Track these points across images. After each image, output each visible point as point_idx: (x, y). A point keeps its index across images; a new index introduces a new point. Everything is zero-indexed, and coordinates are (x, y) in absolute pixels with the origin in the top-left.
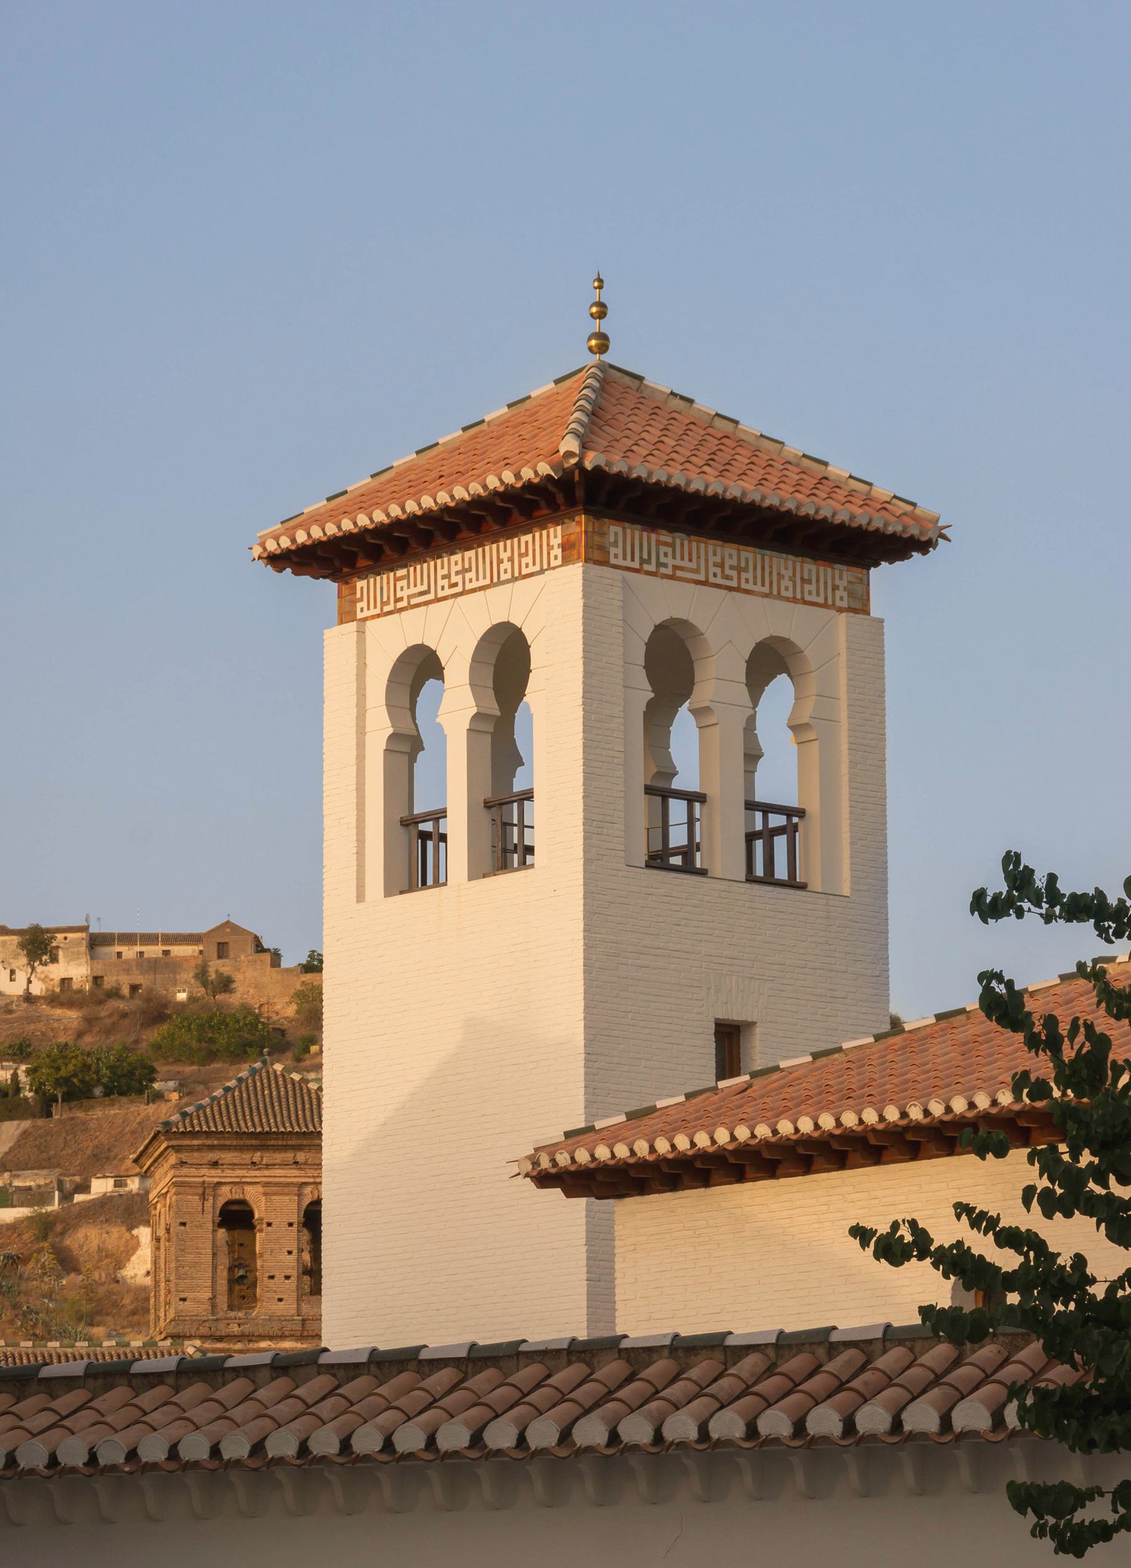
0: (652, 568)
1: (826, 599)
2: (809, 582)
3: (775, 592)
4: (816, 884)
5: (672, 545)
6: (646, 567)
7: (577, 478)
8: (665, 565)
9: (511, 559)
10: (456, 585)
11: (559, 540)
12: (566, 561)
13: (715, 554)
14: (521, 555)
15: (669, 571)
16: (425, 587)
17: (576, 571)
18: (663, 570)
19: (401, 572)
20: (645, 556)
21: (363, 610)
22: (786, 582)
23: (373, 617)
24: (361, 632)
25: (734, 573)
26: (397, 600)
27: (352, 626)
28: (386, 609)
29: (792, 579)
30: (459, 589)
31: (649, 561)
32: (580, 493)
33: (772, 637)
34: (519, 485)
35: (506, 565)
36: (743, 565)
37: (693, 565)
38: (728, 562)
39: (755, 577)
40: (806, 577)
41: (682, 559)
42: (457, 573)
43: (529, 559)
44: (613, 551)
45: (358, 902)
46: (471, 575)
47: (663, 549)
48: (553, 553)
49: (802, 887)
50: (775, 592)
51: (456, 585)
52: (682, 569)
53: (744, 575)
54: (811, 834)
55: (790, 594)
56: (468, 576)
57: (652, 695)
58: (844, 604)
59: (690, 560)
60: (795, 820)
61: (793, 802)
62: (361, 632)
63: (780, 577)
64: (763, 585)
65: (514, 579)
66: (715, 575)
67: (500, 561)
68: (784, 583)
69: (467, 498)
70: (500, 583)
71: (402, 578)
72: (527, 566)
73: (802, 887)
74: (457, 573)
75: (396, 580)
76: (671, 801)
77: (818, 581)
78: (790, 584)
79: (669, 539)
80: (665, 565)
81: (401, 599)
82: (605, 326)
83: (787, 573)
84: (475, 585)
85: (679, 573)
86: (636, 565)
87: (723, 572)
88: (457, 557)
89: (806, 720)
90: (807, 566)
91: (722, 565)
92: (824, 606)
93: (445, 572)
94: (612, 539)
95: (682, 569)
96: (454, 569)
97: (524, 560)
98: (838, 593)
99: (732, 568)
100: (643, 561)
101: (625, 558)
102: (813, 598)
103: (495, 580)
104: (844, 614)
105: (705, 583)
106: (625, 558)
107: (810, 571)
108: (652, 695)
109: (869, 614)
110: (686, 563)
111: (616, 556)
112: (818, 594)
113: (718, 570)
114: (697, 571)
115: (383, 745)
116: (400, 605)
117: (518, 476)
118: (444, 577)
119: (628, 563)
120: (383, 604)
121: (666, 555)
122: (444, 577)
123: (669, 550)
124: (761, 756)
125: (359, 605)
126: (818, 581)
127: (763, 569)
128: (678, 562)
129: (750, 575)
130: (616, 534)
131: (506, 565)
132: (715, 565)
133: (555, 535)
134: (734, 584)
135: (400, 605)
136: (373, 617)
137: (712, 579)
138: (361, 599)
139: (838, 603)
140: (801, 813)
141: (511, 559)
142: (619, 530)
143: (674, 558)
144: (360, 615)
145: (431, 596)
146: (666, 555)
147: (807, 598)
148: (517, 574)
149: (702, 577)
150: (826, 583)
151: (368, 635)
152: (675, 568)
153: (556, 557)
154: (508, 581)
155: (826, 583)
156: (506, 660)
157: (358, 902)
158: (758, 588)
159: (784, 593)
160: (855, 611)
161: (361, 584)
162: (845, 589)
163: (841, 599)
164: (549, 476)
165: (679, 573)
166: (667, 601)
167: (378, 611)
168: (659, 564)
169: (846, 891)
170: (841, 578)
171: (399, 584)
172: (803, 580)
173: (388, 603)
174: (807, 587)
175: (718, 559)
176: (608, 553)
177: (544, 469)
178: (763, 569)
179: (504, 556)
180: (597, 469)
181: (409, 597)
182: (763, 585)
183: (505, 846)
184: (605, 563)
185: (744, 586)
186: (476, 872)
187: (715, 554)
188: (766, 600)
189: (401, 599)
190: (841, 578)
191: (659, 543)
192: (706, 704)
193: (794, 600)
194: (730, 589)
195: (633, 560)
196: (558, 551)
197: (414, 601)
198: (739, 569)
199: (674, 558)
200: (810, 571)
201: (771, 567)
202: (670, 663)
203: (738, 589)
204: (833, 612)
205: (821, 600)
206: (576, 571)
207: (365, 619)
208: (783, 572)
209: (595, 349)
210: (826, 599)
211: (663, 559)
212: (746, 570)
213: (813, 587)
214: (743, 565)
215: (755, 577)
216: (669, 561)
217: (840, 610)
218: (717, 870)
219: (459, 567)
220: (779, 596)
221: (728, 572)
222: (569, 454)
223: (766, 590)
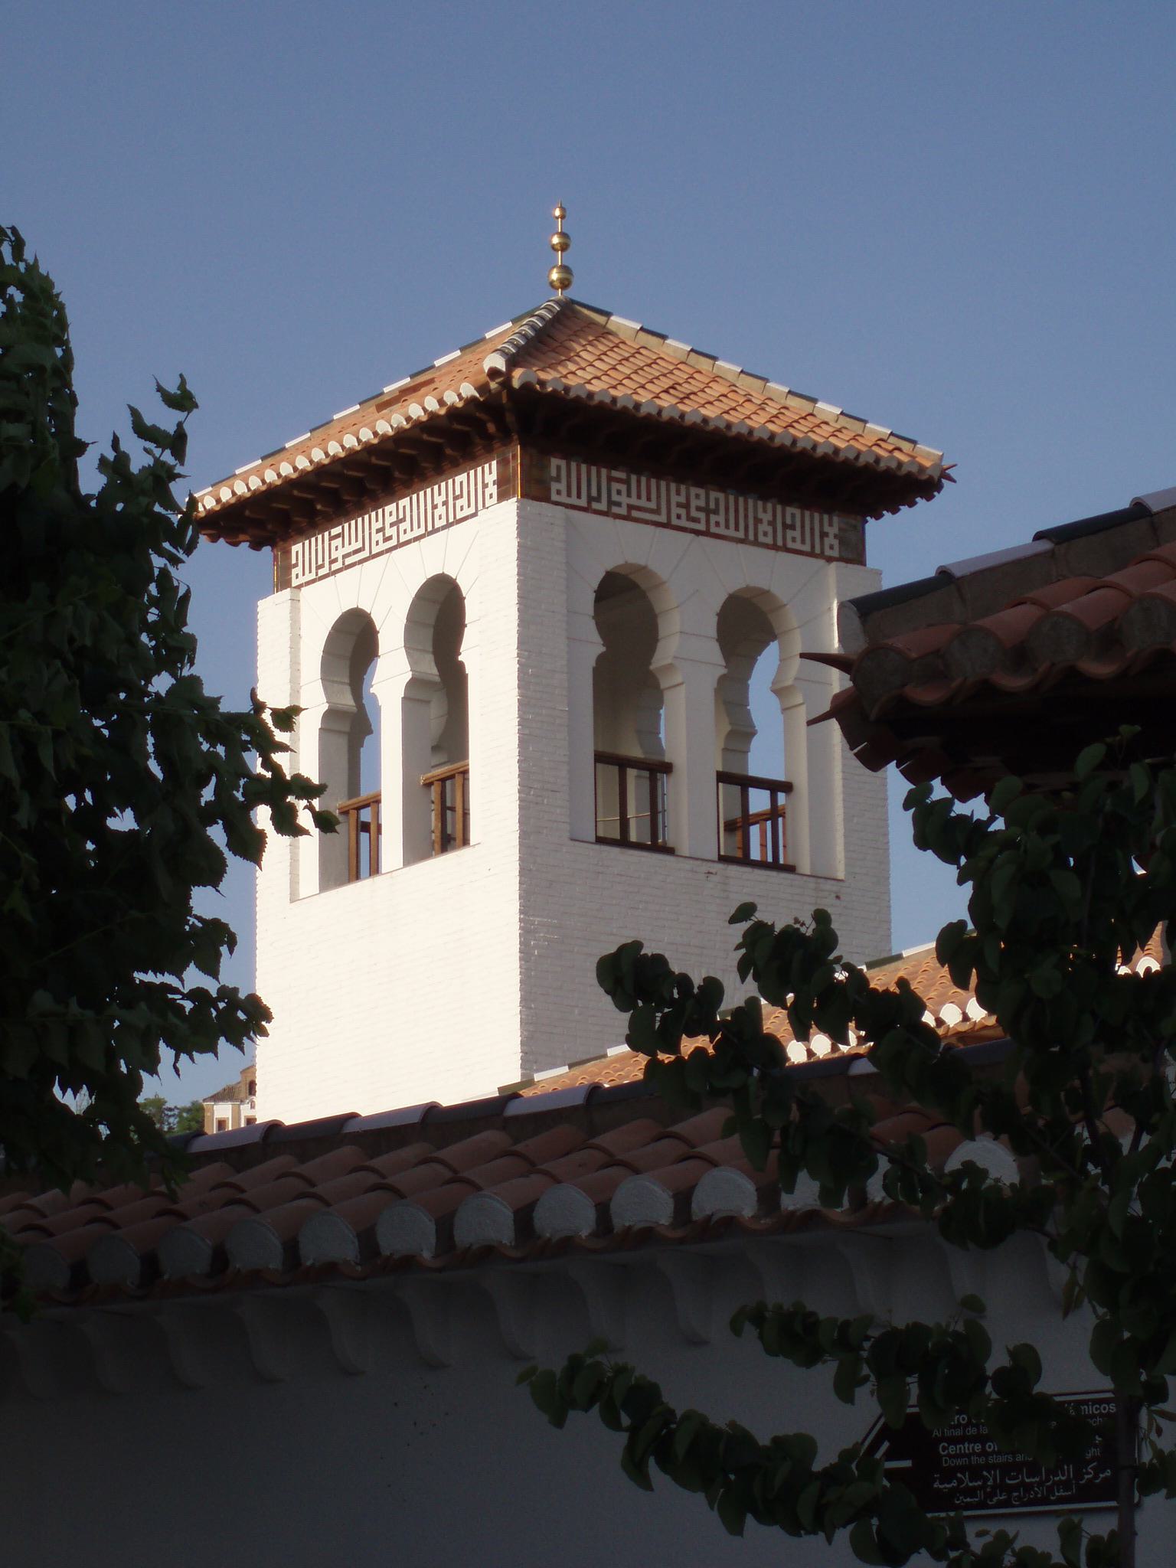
0: (602, 506)
1: (813, 546)
2: (793, 527)
3: (751, 537)
4: (805, 866)
5: (627, 482)
6: (595, 506)
7: (504, 400)
8: (619, 504)
9: (445, 503)
10: (390, 538)
11: (494, 476)
12: (502, 496)
13: (678, 493)
14: (455, 498)
15: (623, 511)
16: (359, 545)
17: (511, 505)
18: (615, 510)
19: (336, 531)
20: (594, 493)
21: (297, 576)
22: (764, 527)
23: (308, 583)
24: (295, 601)
25: (702, 516)
26: (332, 562)
27: (286, 593)
28: (321, 572)
29: (773, 523)
30: (393, 543)
31: (598, 499)
32: (510, 418)
33: (748, 589)
34: (443, 412)
35: (441, 510)
36: (712, 506)
37: (653, 505)
38: (694, 503)
39: (727, 521)
40: (789, 521)
41: (639, 497)
42: (392, 525)
43: (463, 501)
44: (554, 486)
45: (292, 901)
46: (406, 525)
47: (615, 486)
48: (488, 492)
49: (790, 869)
50: (751, 537)
51: (390, 538)
52: (639, 509)
53: (713, 518)
54: (800, 807)
55: (769, 540)
56: (402, 526)
57: (603, 649)
58: (835, 553)
59: (649, 499)
60: (781, 797)
61: (780, 776)
62: (295, 601)
63: (758, 521)
64: (737, 529)
65: (449, 525)
66: (679, 517)
67: (434, 507)
68: (762, 528)
69: (391, 432)
70: (435, 531)
71: (337, 536)
72: (462, 508)
73: (790, 869)
74: (392, 525)
75: (331, 538)
76: (616, 835)
77: (803, 527)
78: (770, 529)
79: (622, 475)
80: (619, 504)
81: (336, 560)
82: (570, 258)
83: (767, 517)
84: (410, 536)
85: (635, 514)
86: (583, 502)
87: (688, 513)
88: (391, 507)
89: (789, 682)
90: (789, 510)
91: (686, 506)
92: (811, 554)
93: (380, 525)
94: (554, 473)
95: (639, 509)
96: (389, 520)
97: (459, 503)
98: (827, 541)
99: (698, 509)
100: (590, 499)
101: (569, 495)
102: (798, 546)
103: (430, 528)
104: (834, 565)
105: (667, 525)
106: (569, 495)
107: (793, 516)
108: (603, 649)
109: (863, 563)
110: (643, 503)
111: (559, 492)
112: (803, 542)
113: (683, 512)
114: (657, 511)
115: (318, 724)
116: (335, 567)
117: (441, 402)
118: (378, 531)
119: (573, 500)
120: (318, 567)
121: (619, 492)
122: (378, 531)
123: (623, 488)
124: (753, 734)
125: (294, 571)
126: (803, 527)
127: (737, 511)
128: (634, 501)
129: (721, 519)
130: (559, 468)
131: (441, 510)
132: (679, 505)
133: (490, 472)
134: (702, 527)
135: (335, 567)
136: (308, 583)
137: (675, 521)
138: (296, 565)
139: (828, 552)
140: (787, 787)
141: (445, 503)
142: (563, 463)
143: (629, 495)
144: (295, 582)
145: (365, 554)
146: (619, 492)
147: (790, 545)
148: (451, 520)
149: (663, 519)
150: (812, 529)
151: (303, 605)
152: (630, 507)
153: (491, 496)
154: (443, 528)
155: (812, 529)
156: (441, 611)
157: (292, 901)
158: (731, 532)
159: (761, 539)
160: (848, 561)
161: (296, 548)
162: (835, 536)
163: (831, 547)
164: (473, 399)
165: (635, 514)
166: (621, 543)
167: (313, 576)
168: (611, 503)
169: (841, 875)
170: (831, 525)
171: (334, 543)
172: (785, 526)
173: (322, 566)
174: (790, 533)
175: (682, 499)
176: (549, 490)
177: (468, 390)
178: (737, 511)
179: (439, 500)
180: (526, 387)
181: (345, 557)
182: (737, 529)
183: (443, 826)
184: (546, 499)
185: (713, 529)
186: (415, 853)
187: (678, 493)
188: (740, 546)
189: (336, 560)
190: (831, 525)
191: (610, 479)
192: (669, 661)
193: (774, 547)
194: (697, 533)
195: (579, 496)
196: (493, 489)
197: (348, 561)
198: (708, 511)
199: (629, 495)
200: (793, 516)
201: (746, 509)
202: (624, 607)
203: (706, 533)
204: (821, 562)
205: (807, 548)
206: (511, 505)
207: (299, 587)
208: (761, 515)
209: (557, 284)
210: (813, 546)
211: (615, 498)
212: (716, 512)
213: (797, 534)
214: (712, 506)
215: (727, 521)
216: (624, 499)
217: (830, 560)
218: (684, 847)
219: (394, 519)
220: (756, 543)
221: (694, 513)
222: (494, 373)
223: (741, 535)
